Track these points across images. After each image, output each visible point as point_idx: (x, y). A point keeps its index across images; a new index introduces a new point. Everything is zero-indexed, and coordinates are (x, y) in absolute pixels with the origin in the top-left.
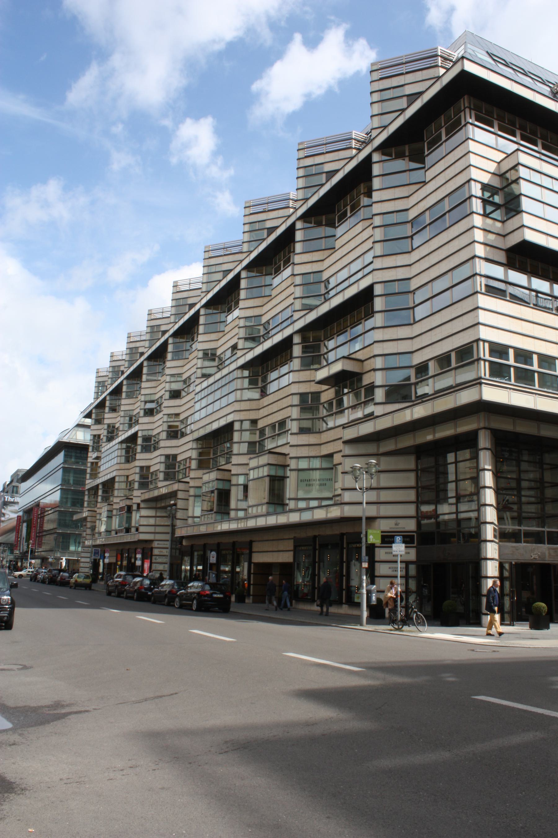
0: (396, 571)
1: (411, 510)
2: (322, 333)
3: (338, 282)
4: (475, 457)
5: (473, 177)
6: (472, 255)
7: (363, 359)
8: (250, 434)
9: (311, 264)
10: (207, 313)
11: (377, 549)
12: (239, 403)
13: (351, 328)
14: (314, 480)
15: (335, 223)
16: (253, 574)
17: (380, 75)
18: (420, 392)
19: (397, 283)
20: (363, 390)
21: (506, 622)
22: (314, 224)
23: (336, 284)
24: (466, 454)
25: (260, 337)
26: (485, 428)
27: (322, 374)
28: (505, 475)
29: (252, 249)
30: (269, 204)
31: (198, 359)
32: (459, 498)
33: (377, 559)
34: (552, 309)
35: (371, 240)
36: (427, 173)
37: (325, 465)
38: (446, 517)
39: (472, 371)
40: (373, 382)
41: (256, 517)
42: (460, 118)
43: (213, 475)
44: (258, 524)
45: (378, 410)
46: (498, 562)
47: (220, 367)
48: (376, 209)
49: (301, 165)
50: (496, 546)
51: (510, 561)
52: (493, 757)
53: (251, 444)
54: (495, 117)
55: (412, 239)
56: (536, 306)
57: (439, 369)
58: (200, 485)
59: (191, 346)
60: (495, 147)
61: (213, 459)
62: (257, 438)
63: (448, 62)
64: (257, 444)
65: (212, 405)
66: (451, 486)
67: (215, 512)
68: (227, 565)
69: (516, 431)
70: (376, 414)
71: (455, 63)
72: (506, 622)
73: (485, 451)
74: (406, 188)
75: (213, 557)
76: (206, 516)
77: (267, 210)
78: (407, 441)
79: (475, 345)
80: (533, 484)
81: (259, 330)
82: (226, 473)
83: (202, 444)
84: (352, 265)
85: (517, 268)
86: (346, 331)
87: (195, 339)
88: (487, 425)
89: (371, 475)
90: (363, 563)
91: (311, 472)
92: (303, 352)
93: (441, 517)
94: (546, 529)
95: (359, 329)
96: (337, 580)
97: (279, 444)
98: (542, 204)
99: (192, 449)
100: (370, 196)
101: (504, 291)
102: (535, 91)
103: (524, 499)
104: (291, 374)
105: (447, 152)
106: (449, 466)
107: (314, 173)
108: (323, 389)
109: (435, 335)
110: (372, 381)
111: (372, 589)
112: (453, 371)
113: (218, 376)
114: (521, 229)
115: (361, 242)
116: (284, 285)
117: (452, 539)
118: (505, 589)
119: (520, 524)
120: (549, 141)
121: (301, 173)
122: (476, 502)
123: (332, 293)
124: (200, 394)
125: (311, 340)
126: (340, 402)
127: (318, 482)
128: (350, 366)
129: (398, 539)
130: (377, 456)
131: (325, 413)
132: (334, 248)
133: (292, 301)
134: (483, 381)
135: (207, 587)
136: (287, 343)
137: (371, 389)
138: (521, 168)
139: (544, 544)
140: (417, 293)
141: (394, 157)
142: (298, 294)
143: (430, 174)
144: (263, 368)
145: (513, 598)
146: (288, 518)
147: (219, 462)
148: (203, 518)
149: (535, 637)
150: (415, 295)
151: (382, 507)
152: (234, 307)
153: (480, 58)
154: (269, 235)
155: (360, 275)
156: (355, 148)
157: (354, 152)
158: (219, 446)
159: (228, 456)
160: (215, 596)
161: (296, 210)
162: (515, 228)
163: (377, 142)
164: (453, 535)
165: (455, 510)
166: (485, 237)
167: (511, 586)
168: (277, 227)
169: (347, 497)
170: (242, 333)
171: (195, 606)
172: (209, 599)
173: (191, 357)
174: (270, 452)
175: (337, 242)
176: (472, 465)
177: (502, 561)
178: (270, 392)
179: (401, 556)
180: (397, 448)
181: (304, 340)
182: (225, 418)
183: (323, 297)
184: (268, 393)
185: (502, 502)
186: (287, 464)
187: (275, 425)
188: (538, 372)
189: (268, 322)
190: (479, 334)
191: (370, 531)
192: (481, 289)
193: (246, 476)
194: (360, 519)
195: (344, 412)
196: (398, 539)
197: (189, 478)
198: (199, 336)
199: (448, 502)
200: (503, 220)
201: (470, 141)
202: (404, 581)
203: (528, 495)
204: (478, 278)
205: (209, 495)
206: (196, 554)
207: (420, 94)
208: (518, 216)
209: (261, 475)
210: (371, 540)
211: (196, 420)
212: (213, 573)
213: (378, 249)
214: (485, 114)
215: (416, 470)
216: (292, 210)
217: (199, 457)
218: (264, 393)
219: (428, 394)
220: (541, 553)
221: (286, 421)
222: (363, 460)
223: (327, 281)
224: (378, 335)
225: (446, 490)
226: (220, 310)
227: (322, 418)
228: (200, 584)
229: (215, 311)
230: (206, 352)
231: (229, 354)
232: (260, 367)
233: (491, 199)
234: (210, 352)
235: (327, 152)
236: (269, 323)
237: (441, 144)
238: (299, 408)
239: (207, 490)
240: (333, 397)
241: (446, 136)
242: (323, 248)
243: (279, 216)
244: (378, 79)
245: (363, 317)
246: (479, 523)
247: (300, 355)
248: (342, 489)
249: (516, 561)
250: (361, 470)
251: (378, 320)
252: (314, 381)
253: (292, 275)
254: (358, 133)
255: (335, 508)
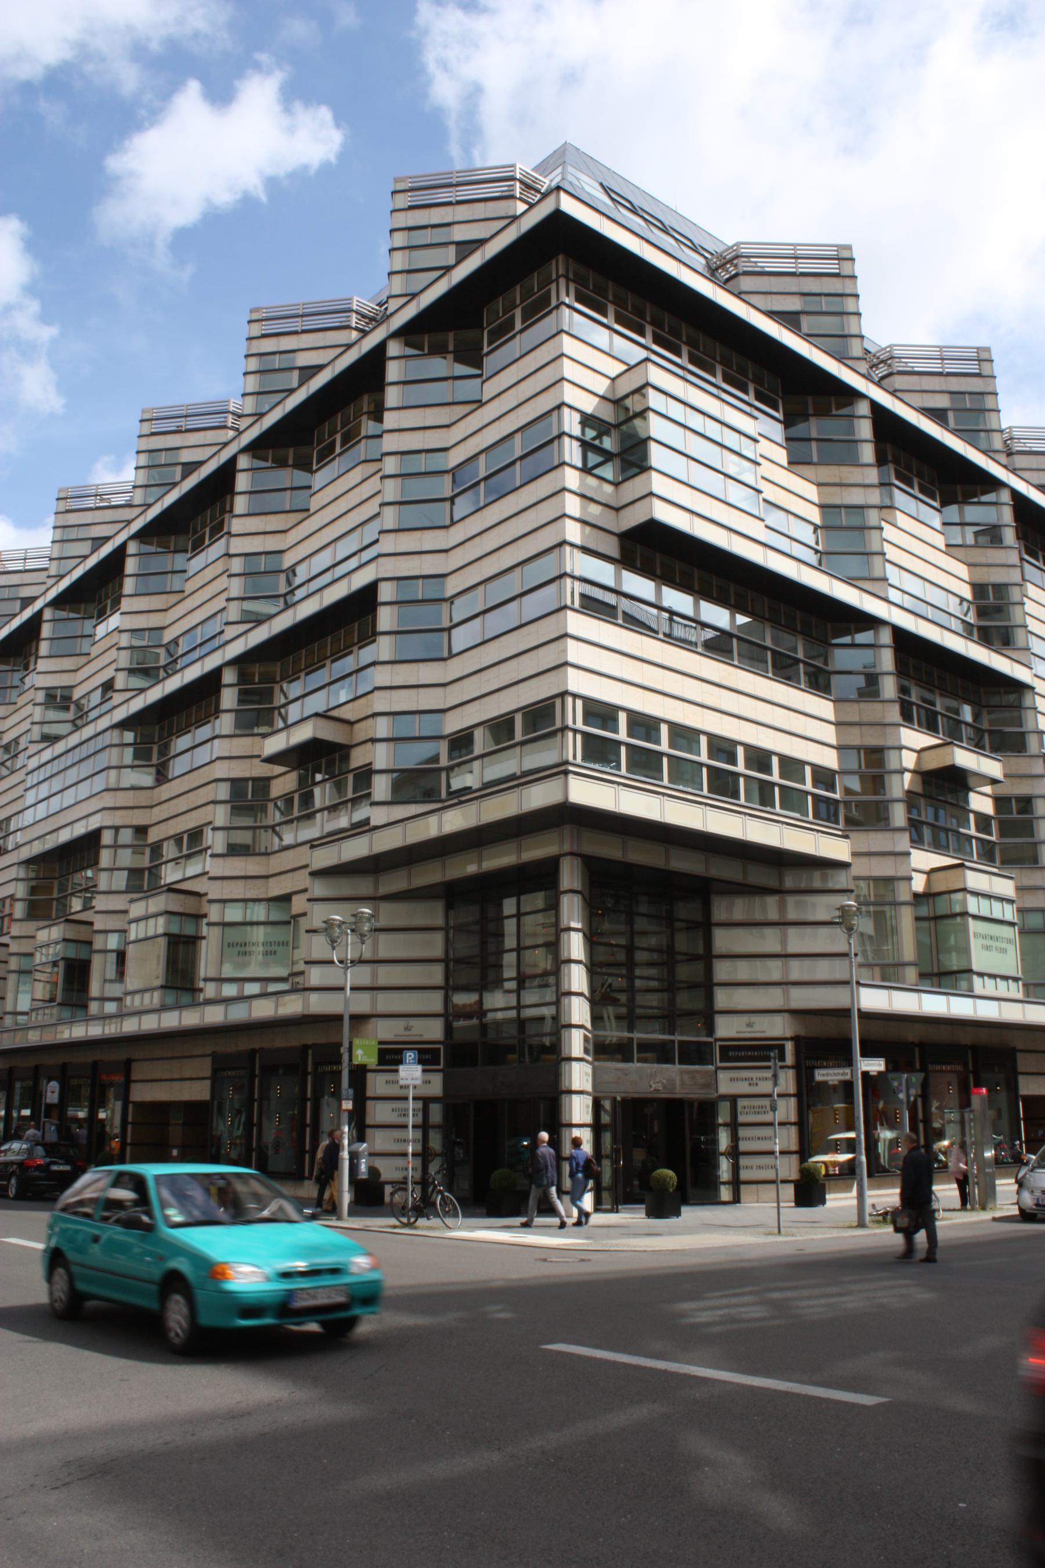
0: (404, 1115)
1: (434, 1002)
2: (277, 668)
3: (313, 574)
4: (553, 906)
5: (568, 399)
6: (559, 540)
7: (353, 719)
8: (134, 853)
9: (262, 536)
10: (56, 618)
11: (369, 1075)
12: (113, 793)
13: (333, 661)
14: (253, 944)
15: (312, 464)
16: (132, 1123)
17: (410, 201)
18: (457, 784)
19: (420, 581)
20: (350, 778)
21: (604, 1207)
22: (272, 462)
23: (309, 577)
24: (538, 900)
25: (158, 668)
26: (572, 854)
27: (275, 744)
28: (605, 940)
29: (151, 501)
30: (188, 419)
31: (34, 705)
32: (522, 981)
33: (369, 1093)
34: (696, 644)
35: (378, 500)
36: (485, 386)
37: (275, 916)
38: (500, 1015)
39: (550, 750)
40: (370, 764)
41: (140, 1013)
42: (548, 294)
43: (56, 932)
44: (142, 1028)
45: (378, 816)
46: (591, 1098)
47: (79, 722)
48: (390, 443)
49: (254, 351)
50: (588, 1069)
51: (613, 1095)
52: (578, 1454)
53: (135, 873)
54: (611, 298)
55: (453, 503)
56: (670, 638)
57: (492, 742)
58: (30, 950)
59: (22, 680)
60: (607, 350)
61: (57, 899)
62: (145, 862)
63: (533, 192)
64: (146, 873)
65: (59, 795)
66: (509, 959)
67: (59, 1004)
68: (81, 1107)
69: (628, 861)
70: (373, 823)
71: (545, 196)
72: (604, 1207)
73: (570, 895)
74: (446, 409)
75: (53, 1092)
76: (40, 1012)
77: (183, 429)
78: (430, 875)
79: (558, 702)
80: (655, 956)
81: (158, 655)
82: (83, 927)
83: (37, 871)
84: (340, 544)
85: (675, 583)
86: (324, 666)
87: (32, 667)
88: (575, 849)
89: (362, 935)
90: (343, 1102)
91: (249, 928)
92: (241, 701)
93: (490, 1016)
94: (677, 1037)
95: (348, 663)
96: (294, 1134)
97: (189, 874)
98: (685, 459)
99: (16, 880)
100: (379, 419)
101: (614, 608)
102: (679, 261)
103: (638, 983)
104: (216, 742)
105: (524, 352)
106: (506, 922)
107: (277, 367)
108: (276, 773)
109: (488, 680)
110: (367, 762)
111: (361, 1149)
112: (518, 749)
113: (74, 740)
114: (647, 499)
115: (358, 502)
116: (209, 574)
117: (510, 1057)
118: (603, 1147)
119: (631, 1029)
120: (701, 349)
121: (253, 364)
122: (554, 988)
123: (300, 594)
124: (36, 773)
125: (257, 680)
126: (307, 799)
127: (261, 948)
128: (328, 732)
129: (410, 1056)
130: (373, 902)
131: (278, 818)
132: (308, 510)
133: (224, 604)
134: (571, 768)
135: (40, 1151)
136: (211, 682)
137: (366, 775)
138: (651, 392)
139: (674, 1063)
140: (458, 602)
141: (426, 351)
142: (234, 592)
143: (491, 388)
144: (162, 729)
145: (617, 1162)
146: (203, 1016)
147: (71, 907)
148: (34, 1014)
149: (654, 1231)
150: (453, 606)
151: (381, 996)
152: (111, 609)
153: (589, 194)
154: (184, 477)
155: (353, 563)
156: (356, 329)
157: (355, 335)
158: (70, 876)
159: (89, 895)
160: (55, 1168)
161: (240, 433)
162: (636, 497)
163: (398, 321)
164: (511, 1049)
165: (514, 1003)
166: (583, 509)
167: (614, 1140)
168: (200, 464)
169: (316, 976)
170: (124, 659)
171: (14, 1190)
172: (43, 1175)
173: (21, 701)
174: (171, 889)
175: (313, 498)
176: (547, 921)
177: (598, 1095)
178: (176, 775)
179: (415, 1087)
180: (410, 888)
181: (243, 678)
182: (83, 822)
183: (282, 600)
184: (170, 777)
185: (599, 989)
186: (203, 912)
187: (182, 837)
188: (669, 756)
189: (175, 641)
190: (566, 683)
191: (357, 1042)
192: (573, 602)
193: (123, 934)
194: (339, 1018)
195: (315, 817)
196: (410, 1056)
197: (8, 936)
198: (39, 661)
199: (502, 987)
200: (616, 481)
201: (565, 337)
202: (419, 1134)
203: (646, 976)
204: (569, 581)
205: (49, 970)
206: (18, 1085)
207: (481, 243)
208: (643, 477)
209: (151, 933)
210: (359, 1059)
211: (26, 824)
212: (52, 1124)
213: (390, 518)
214: (592, 291)
215: (446, 929)
216: (231, 434)
217: (31, 895)
218: (162, 776)
219: (470, 788)
220: (668, 1080)
221: (202, 830)
222: (348, 907)
223: (292, 570)
224: (381, 676)
225: (499, 966)
226: (82, 612)
227: (273, 827)
228: (24, 1146)
229: (72, 615)
230: (52, 692)
231: (96, 697)
232: (157, 727)
233: (597, 442)
234: (59, 693)
235: (304, 332)
236: (177, 644)
237: (514, 336)
238: (229, 806)
239: (44, 959)
240: (294, 789)
241: (523, 322)
242: (288, 508)
243: (207, 443)
244: (406, 207)
245: (356, 641)
246: (557, 1026)
247: (235, 706)
248: (307, 963)
249: (624, 1095)
250: (343, 927)
251: (383, 648)
252: (259, 756)
253: (225, 555)
254: (363, 301)
255: (293, 997)
